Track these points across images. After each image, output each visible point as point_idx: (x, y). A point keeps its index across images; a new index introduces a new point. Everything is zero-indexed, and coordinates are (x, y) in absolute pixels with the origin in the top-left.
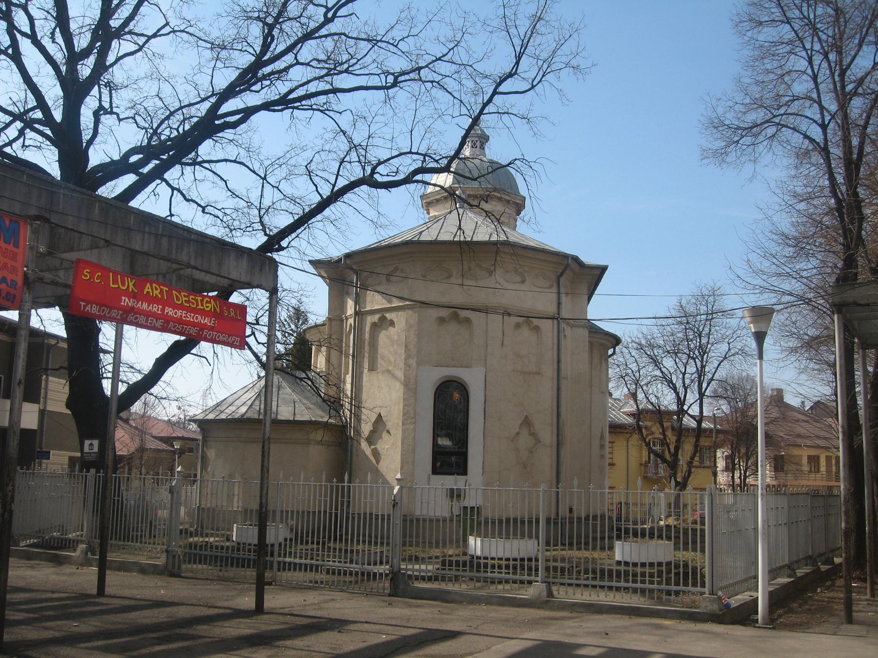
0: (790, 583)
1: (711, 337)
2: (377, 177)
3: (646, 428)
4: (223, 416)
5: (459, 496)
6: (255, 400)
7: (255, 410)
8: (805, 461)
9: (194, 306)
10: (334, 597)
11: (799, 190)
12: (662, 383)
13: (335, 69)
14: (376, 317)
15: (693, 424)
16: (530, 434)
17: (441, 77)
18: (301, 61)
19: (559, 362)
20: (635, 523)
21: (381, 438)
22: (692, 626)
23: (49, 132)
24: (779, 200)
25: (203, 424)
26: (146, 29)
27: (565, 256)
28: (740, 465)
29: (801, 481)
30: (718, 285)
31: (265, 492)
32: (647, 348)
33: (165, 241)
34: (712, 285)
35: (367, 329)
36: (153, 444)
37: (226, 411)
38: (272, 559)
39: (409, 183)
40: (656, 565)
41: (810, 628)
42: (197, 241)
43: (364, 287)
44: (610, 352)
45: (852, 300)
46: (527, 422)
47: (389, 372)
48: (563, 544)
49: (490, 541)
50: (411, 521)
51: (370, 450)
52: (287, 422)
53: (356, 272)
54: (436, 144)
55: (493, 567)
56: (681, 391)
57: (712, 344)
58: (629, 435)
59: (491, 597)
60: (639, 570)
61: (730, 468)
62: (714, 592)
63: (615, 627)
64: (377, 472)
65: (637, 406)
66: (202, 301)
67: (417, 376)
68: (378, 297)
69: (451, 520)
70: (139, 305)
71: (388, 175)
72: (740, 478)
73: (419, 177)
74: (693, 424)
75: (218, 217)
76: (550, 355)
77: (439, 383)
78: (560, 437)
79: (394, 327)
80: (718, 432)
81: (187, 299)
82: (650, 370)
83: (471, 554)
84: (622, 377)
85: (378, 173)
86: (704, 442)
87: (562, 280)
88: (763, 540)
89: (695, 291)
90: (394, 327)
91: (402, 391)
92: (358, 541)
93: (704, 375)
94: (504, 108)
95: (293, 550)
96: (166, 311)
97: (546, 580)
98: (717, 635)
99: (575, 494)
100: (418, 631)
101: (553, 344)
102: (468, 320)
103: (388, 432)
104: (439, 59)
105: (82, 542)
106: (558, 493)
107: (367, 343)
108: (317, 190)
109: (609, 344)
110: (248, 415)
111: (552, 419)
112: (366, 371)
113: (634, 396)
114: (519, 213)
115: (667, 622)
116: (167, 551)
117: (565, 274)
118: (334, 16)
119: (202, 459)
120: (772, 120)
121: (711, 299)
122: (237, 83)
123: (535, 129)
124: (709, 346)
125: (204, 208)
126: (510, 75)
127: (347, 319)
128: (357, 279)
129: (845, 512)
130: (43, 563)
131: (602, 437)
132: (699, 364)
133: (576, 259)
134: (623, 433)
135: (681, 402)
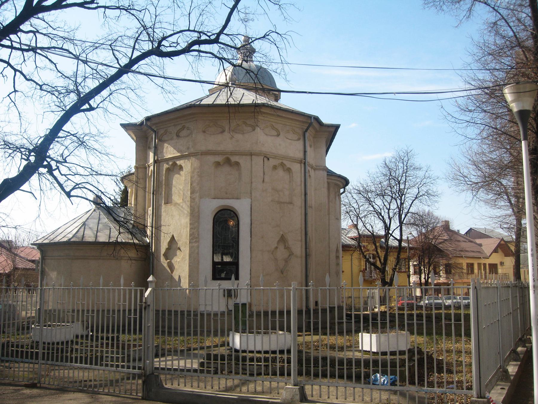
2: (163, 49)
3: (364, 247)
4: (56, 240)
6: (80, 228)
8: (465, 267)
19: (306, 194)
20: (358, 310)
21: (176, 255)
25: (41, 247)
27: (309, 117)
30: (410, 149)
32: (364, 193)
34: (406, 149)
43: (162, 141)
44: (342, 190)
46: (283, 239)
49: (247, 335)
50: (196, 315)
52: (104, 243)
53: (155, 132)
56: (387, 221)
58: (352, 252)
62: (482, 395)
64: (172, 278)
65: (358, 232)
71: (170, 46)
72: (425, 278)
73: (196, 47)
74: (396, 244)
76: (299, 190)
77: (216, 212)
80: (411, 249)
84: (347, 212)
85: (163, 45)
87: (307, 134)
90: (183, 171)
101: (301, 181)
102: (237, 164)
103: (179, 249)
106: (307, 291)
111: (301, 237)
113: (356, 226)
117: (309, 131)
121: (406, 159)
123: (285, 14)
124: (405, 190)
127: (149, 167)
128: (155, 136)
131: (337, 251)
132: (399, 201)
133: (317, 119)
135: (387, 228)
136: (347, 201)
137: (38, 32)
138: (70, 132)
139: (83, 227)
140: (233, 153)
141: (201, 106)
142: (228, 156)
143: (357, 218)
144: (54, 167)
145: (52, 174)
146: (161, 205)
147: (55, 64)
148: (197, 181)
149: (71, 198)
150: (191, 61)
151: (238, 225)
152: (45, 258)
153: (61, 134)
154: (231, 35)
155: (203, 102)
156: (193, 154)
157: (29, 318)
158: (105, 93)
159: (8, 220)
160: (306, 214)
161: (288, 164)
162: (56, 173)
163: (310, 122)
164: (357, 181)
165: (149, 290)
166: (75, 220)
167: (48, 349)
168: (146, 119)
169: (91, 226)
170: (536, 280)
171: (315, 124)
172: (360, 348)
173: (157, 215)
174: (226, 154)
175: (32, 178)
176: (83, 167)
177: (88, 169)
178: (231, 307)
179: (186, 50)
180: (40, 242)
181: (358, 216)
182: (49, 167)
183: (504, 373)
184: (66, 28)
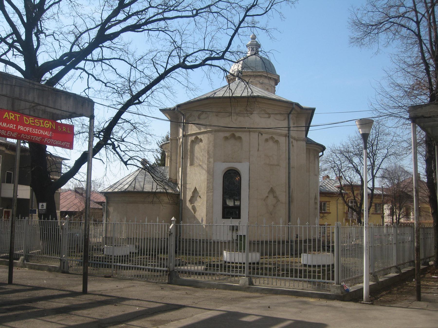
0: (395, 276)
1: (378, 146)
4: (116, 190)
5: (237, 230)
6: (132, 182)
7: (132, 186)
9: (39, 125)
10: (135, 285)
11: (409, 60)
12: (354, 171)
13: (167, 9)
14: (193, 138)
17: (220, 10)
18: (152, 5)
19: (289, 159)
22: (324, 302)
23: (20, 47)
24: (397, 67)
27: (292, 103)
28: (396, 213)
29: (429, 221)
31: (87, 227)
33: (17, 90)
35: (189, 143)
36: (92, 205)
37: (119, 187)
38: (111, 264)
39: (203, 66)
40: (321, 266)
41: (395, 303)
42: (39, 89)
44: (321, 154)
45: (420, 115)
46: (272, 191)
47: (200, 165)
48: (279, 254)
50: (211, 243)
51: (191, 206)
52: (148, 193)
53: (183, 115)
54: (216, 44)
57: (378, 150)
59: (220, 284)
61: (392, 214)
62: (339, 283)
63: (278, 303)
64: (194, 217)
66: (43, 123)
67: (214, 168)
68: (194, 127)
69: (233, 242)
70: (8, 126)
72: (396, 219)
73: (209, 62)
75: (114, 89)
78: (290, 198)
80: (384, 195)
81: (33, 121)
82: (347, 163)
83: (225, 260)
86: (376, 201)
88: (366, 253)
91: (206, 175)
92: (144, 254)
93: (375, 166)
95: (134, 259)
96: (19, 128)
97: (249, 275)
98: (335, 308)
99: (188, 226)
100: (162, 305)
101: (286, 150)
102: (240, 138)
103: (200, 197)
105: (22, 255)
108: (157, 71)
109: (319, 150)
110: (129, 189)
112: (188, 165)
114: (276, 84)
115: (311, 300)
116: (61, 260)
119: (107, 213)
120: (389, 20)
122: (111, 16)
123: (271, 36)
124: (377, 151)
125: (106, 84)
126: (253, 6)
127: (179, 139)
129: (417, 237)
130: (4, 266)
131: (316, 198)
133: (297, 105)
134: (333, 197)
136: (332, 159)
139: (134, 181)
141: (214, 98)
142: (233, 132)
143: (339, 172)
144: (116, 146)
145: (115, 150)
147: (115, 69)
148: (212, 150)
149: (127, 166)
150: (206, 71)
151: (240, 179)
154: (233, 52)
157: (98, 243)
158: (149, 92)
160: (289, 173)
161: (276, 137)
162: (118, 149)
163: (292, 107)
164: (340, 144)
165: (172, 225)
166: (129, 176)
169: (140, 180)
170: (367, 224)
171: (296, 108)
172: (302, 263)
174: (232, 131)
177: (138, 146)
178: (235, 238)
179: (203, 64)
180: (105, 191)
181: (340, 171)
182: (113, 144)
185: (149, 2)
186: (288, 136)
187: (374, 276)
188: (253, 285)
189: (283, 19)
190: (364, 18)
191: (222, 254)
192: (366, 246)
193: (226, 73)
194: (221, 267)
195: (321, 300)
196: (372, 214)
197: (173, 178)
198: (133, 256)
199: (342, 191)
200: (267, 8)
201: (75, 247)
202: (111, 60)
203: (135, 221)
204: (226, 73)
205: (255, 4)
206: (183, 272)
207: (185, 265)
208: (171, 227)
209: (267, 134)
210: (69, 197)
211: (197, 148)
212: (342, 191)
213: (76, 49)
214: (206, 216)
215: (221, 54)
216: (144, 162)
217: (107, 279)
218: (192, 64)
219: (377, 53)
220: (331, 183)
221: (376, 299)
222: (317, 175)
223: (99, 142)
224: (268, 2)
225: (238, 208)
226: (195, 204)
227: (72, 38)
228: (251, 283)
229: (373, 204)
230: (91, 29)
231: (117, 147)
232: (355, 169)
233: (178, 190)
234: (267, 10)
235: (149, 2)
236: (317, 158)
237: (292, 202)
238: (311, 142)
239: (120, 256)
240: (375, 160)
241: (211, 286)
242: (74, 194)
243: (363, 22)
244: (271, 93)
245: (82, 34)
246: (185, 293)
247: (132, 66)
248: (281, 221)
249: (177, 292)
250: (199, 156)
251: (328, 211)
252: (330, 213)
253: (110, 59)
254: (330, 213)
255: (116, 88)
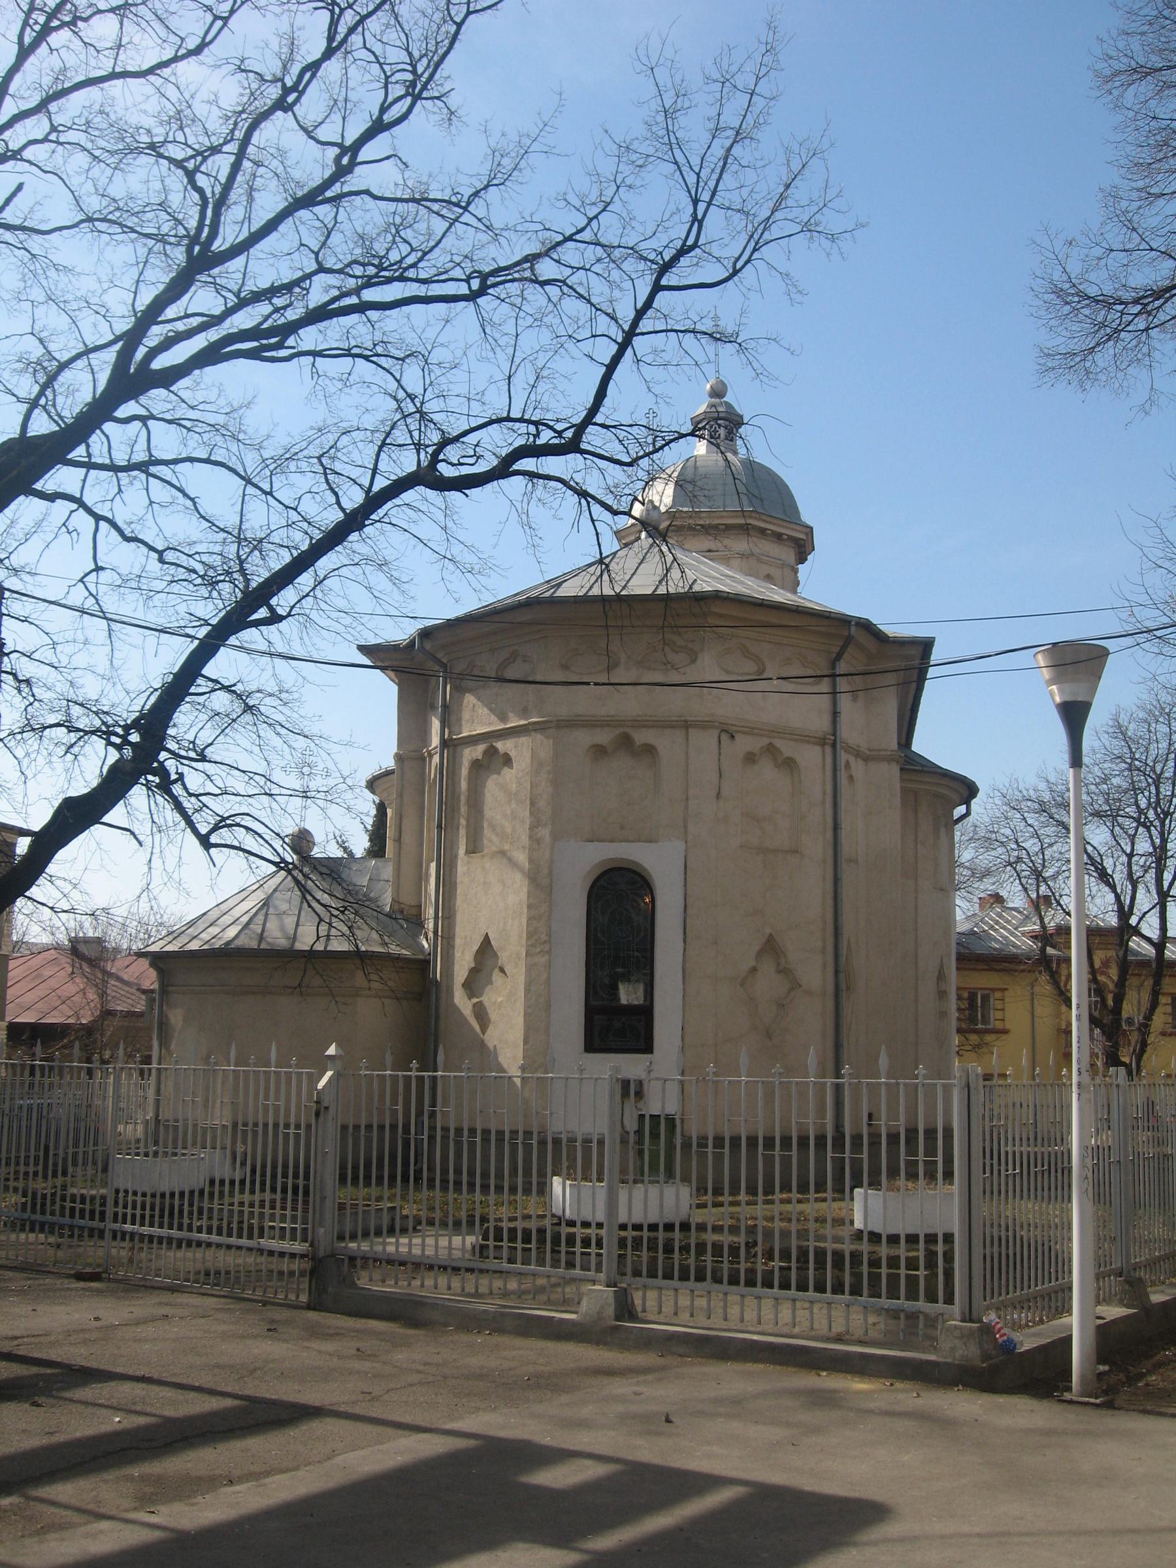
4: (194, 946)
5: (639, 1094)
12: (1090, 875)
15: (1150, 951)
16: (779, 972)
17: (569, 271)
18: (328, 265)
19: (836, 828)
22: (908, 1396)
25: (159, 960)
26: (42, 221)
27: (844, 621)
35: (464, 772)
37: (203, 935)
38: (102, 1225)
43: (459, 690)
46: (771, 948)
47: (503, 853)
48: (803, 1188)
49: (593, 1187)
50: (542, 1143)
51: (471, 1007)
55: (586, 1242)
59: (503, 1315)
60: (884, 1251)
62: (975, 1315)
74: (1150, 951)
75: (195, 571)
77: (598, 872)
78: (842, 976)
79: (512, 768)
88: (1083, 1193)
89: (1145, 697)
90: (512, 768)
91: (525, 889)
94: (688, 322)
100: (229, 1402)
101: (824, 793)
102: (650, 750)
103: (502, 970)
104: (570, 238)
106: (838, 1088)
107: (463, 799)
108: (338, 503)
109: (955, 797)
110: (238, 943)
112: (462, 851)
114: (802, 559)
115: (860, 1385)
117: (846, 656)
118: (353, 164)
119: (160, 1028)
123: (755, 364)
125: (160, 553)
126: (683, 251)
127: (431, 756)
131: (941, 976)
133: (866, 626)
134: (1016, 971)
135: (1124, 913)
136: (1008, 832)
137: (153, 417)
138: (220, 680)
140: (641, 724)
141: (554, 602)
143: (1037, 879)
146: (455, 857)
149: (213, 851)
151: (653, 901)
152: (170, 988)
153: (201, 685)
155: (562, 592)
156: (537, 727)
158: (305, 580)
159: (75, 895)
160: (836, 881)
161: (787, 748)
162: (177, 789)
165: (329, 1074)
167: (143, 1208)
168: (419, 635)
170: (1083, 1070)
172: (858, 1224)
173: (447, 884)
175: (132, 792)
176: (244, 772)
177: (257, 778)
178: (631, 1125)
179: (503, 470)
181: (1038, 875)
183: (1127, 1287)
184: (222, 402)
185: (317, 254)
186: (831, 741)
187: (1129, 1282)
188: (632, 1316)
189: (798, 297)
190: (1092, 277)
191: (543, 1189)
192: (1083, 1165)
193: (588, 503)
194: (542, 1241)
195: (899, 1385)
196: (1163, 1034)
197: (407, 899)
198: (221, 1193)
199: (1050, 950)
200: (737, 259)
201: (37, 1158)
202: (180, 467)
203: (273, 1062)
204: (588, 503)
205: (690, 242)
206: (368, 1261)
207: (415, 1230)
208: (321, 1085)
209: (753, 734)
210: (47, 973)
211: (492, 787)
212: (1050, 950)
213: (41, 425)
214: (526, 1042)
215: (569, 434)
216: (301, 841)
217: (81, 1284)
218: (465, 470)
219: (1147, 406)
220: (1008, 922)
221: (1132, 1380)
222: (946, 888)
223: (117, 761)
224: (744, 238)
225: (645, 1013)
226: (485, 999)
227: (27, 387)
228: (625, 1310)
229: (1163, 1000)
230: (98, 348)
231: (175, 781)
232: (1096, 868)
233: (426, 946)
234: (738, 266)
235: (317, 254)
236: (946, 825)
237: (848, 988)
238: (923, 766)
239: (182, 1194)
240: (1169, 833)
241: (471, 1322)
242: (65, 961)
243: (1093, 291)
244: (783, 588)
245: (63, 366)
246: (354, 1352)
247: (248, 481)
248: (812, 1060)
249: (329, 1346)
250: (498, 817)
251: (999, 1025)
252: (1005, 1032)
253: (176, 462)
254: (1005, 1032)
255: (200, 569)
